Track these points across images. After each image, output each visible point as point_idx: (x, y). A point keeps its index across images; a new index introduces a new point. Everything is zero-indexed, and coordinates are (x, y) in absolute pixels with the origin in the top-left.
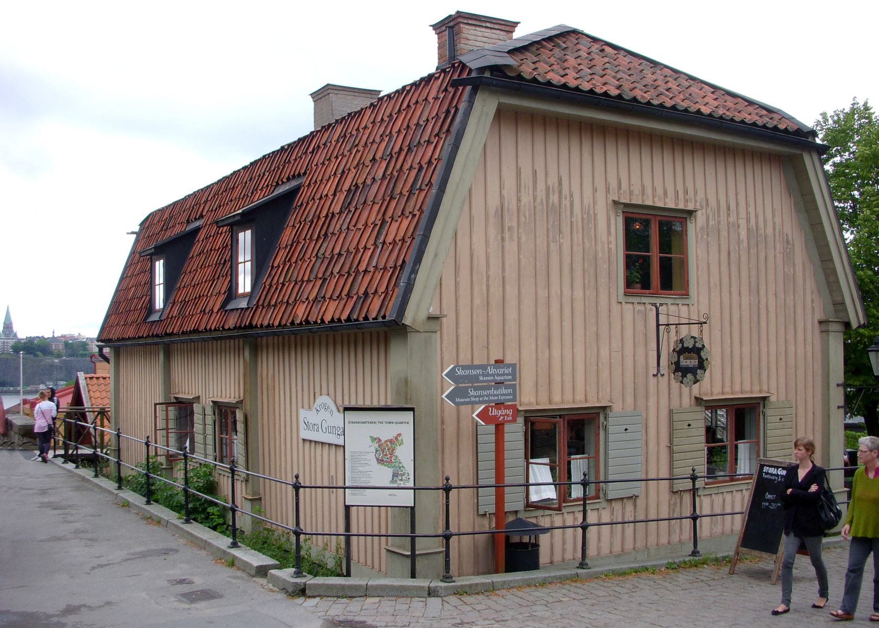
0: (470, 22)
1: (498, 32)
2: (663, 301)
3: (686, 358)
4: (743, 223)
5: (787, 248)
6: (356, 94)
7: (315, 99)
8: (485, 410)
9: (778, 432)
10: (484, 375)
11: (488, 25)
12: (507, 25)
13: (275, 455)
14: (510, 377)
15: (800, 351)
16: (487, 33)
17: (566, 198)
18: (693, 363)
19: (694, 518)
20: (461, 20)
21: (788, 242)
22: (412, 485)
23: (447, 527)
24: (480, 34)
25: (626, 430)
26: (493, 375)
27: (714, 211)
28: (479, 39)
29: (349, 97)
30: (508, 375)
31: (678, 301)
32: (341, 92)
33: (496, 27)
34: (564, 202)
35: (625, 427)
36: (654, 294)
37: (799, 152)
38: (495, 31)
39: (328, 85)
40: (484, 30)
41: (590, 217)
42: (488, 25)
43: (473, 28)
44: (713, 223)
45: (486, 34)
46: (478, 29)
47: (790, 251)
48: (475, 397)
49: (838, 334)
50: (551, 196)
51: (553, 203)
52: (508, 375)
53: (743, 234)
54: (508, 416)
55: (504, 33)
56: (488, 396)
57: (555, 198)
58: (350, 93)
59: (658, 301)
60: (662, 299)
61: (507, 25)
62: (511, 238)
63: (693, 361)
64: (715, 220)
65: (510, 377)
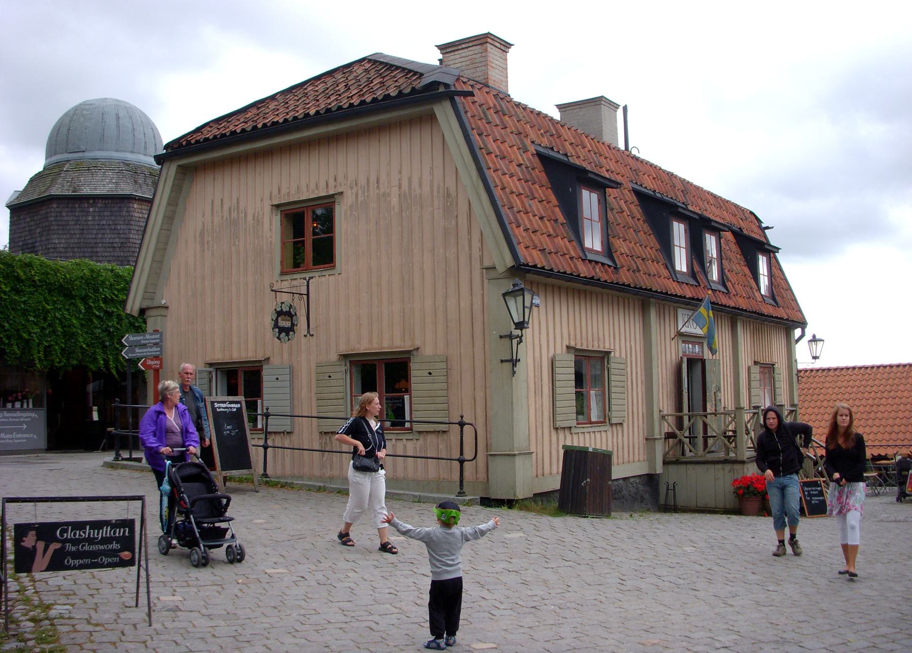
0: (448, 50)
1: (473, 48)
2: (311, 275)
3: (282, 320)
4: (395, 191)
5: (447, 201)
6: (581, 106)
7: (616, 109)
8: (145, 361)
9: (619, 390)
10: (144, 340)
11: (463, 46)
12: (480, 39)
13: (632, 401)
14: (158, 340)
15: (465, 304)
16: (464, 53)
17: (242, 212)
18: (287, 324)
19: (462, 462)
20: (489, 40)
21: (449, 195)
22: (688, 435)
23: (462, 453)
24: (458, 56)
25: (277, 379)
26: (149, 339)
27: (364, 187)
28: (457, 61)
29: (575, 111)
30: (157, 339)
31: (324, 273)
32: (568, 109)
33: (471, 44)
34: (241, 215)
35: (276, 377)
36: (307, 270)
37: (428, 107)
38: (471, 49)
39: (602, 97)
40: (461, 51)
41: (258, 221)
42: (463, 46)
43: (453, 54)
44: (363, 198)
45: (463, 55)
46: (456, 53)
47: (451, 204)
48: (139, 353)
49: (501, 281)
50: (233, 213)
51: (234, 219)
52: (157, 339)
53: (395, 200)
54: (157, 364)
55: (479, 47)
56: (146, 352)
57: (234, 215)
58: (576, 107)
59: (307, 276)
60: (330, 271)
61: (480, 39)
62: (208, 248)
63: (287, 322)
64: (364, 196)
65: (158, 340)
